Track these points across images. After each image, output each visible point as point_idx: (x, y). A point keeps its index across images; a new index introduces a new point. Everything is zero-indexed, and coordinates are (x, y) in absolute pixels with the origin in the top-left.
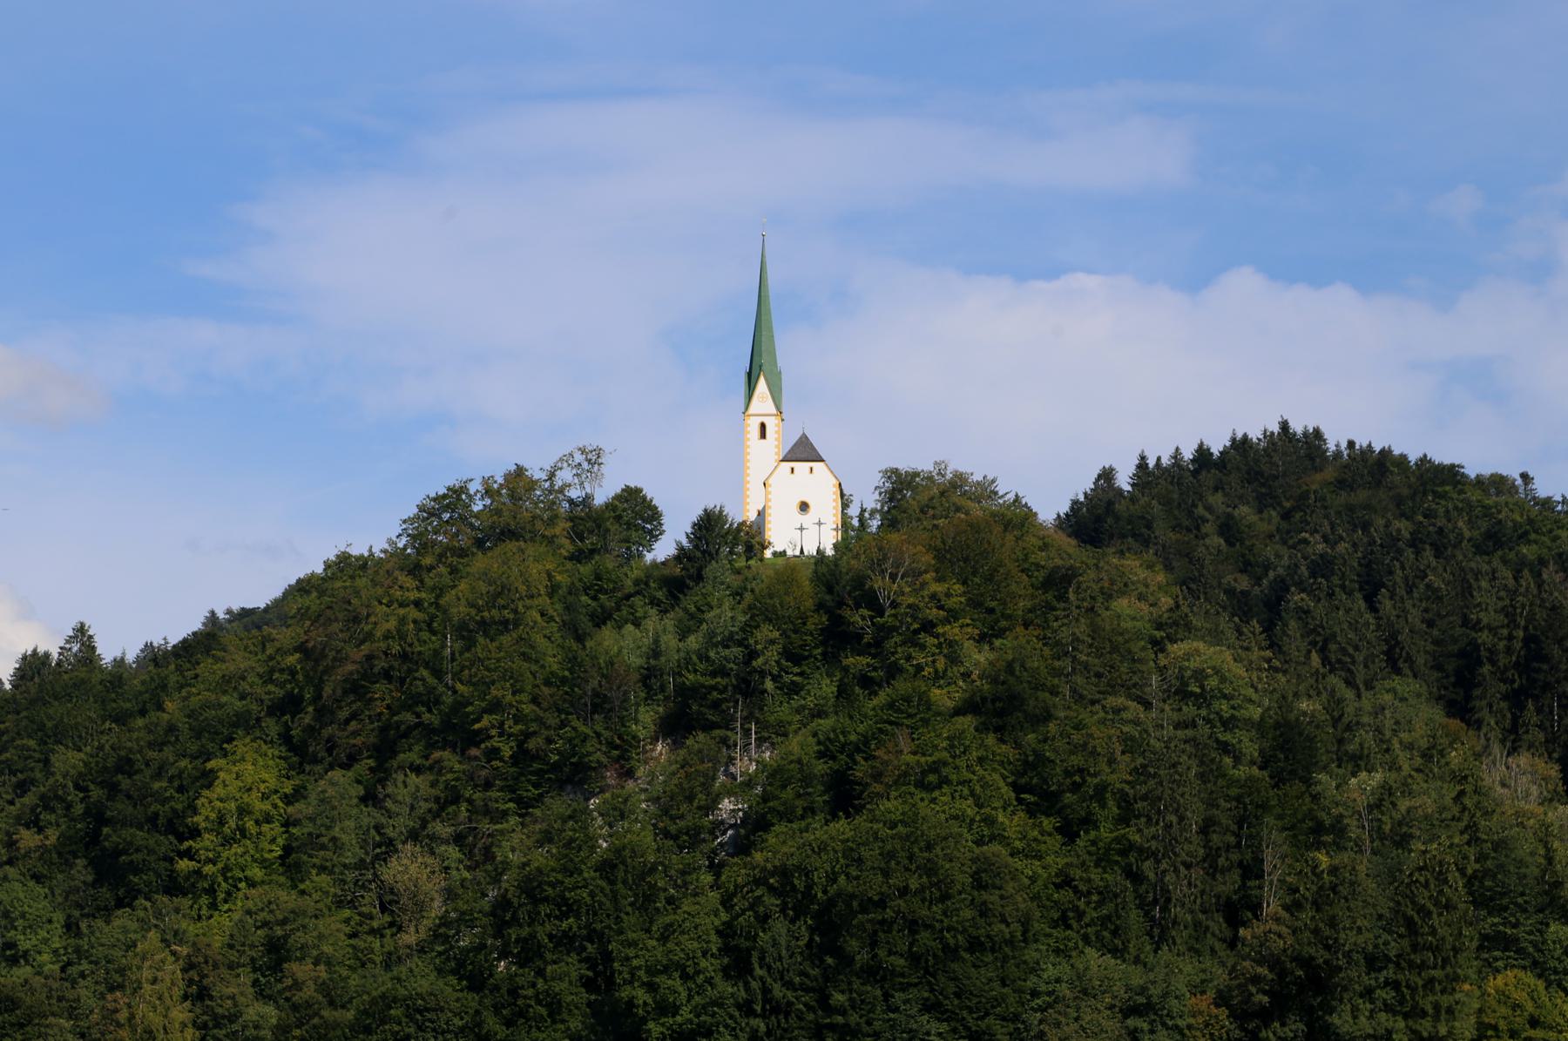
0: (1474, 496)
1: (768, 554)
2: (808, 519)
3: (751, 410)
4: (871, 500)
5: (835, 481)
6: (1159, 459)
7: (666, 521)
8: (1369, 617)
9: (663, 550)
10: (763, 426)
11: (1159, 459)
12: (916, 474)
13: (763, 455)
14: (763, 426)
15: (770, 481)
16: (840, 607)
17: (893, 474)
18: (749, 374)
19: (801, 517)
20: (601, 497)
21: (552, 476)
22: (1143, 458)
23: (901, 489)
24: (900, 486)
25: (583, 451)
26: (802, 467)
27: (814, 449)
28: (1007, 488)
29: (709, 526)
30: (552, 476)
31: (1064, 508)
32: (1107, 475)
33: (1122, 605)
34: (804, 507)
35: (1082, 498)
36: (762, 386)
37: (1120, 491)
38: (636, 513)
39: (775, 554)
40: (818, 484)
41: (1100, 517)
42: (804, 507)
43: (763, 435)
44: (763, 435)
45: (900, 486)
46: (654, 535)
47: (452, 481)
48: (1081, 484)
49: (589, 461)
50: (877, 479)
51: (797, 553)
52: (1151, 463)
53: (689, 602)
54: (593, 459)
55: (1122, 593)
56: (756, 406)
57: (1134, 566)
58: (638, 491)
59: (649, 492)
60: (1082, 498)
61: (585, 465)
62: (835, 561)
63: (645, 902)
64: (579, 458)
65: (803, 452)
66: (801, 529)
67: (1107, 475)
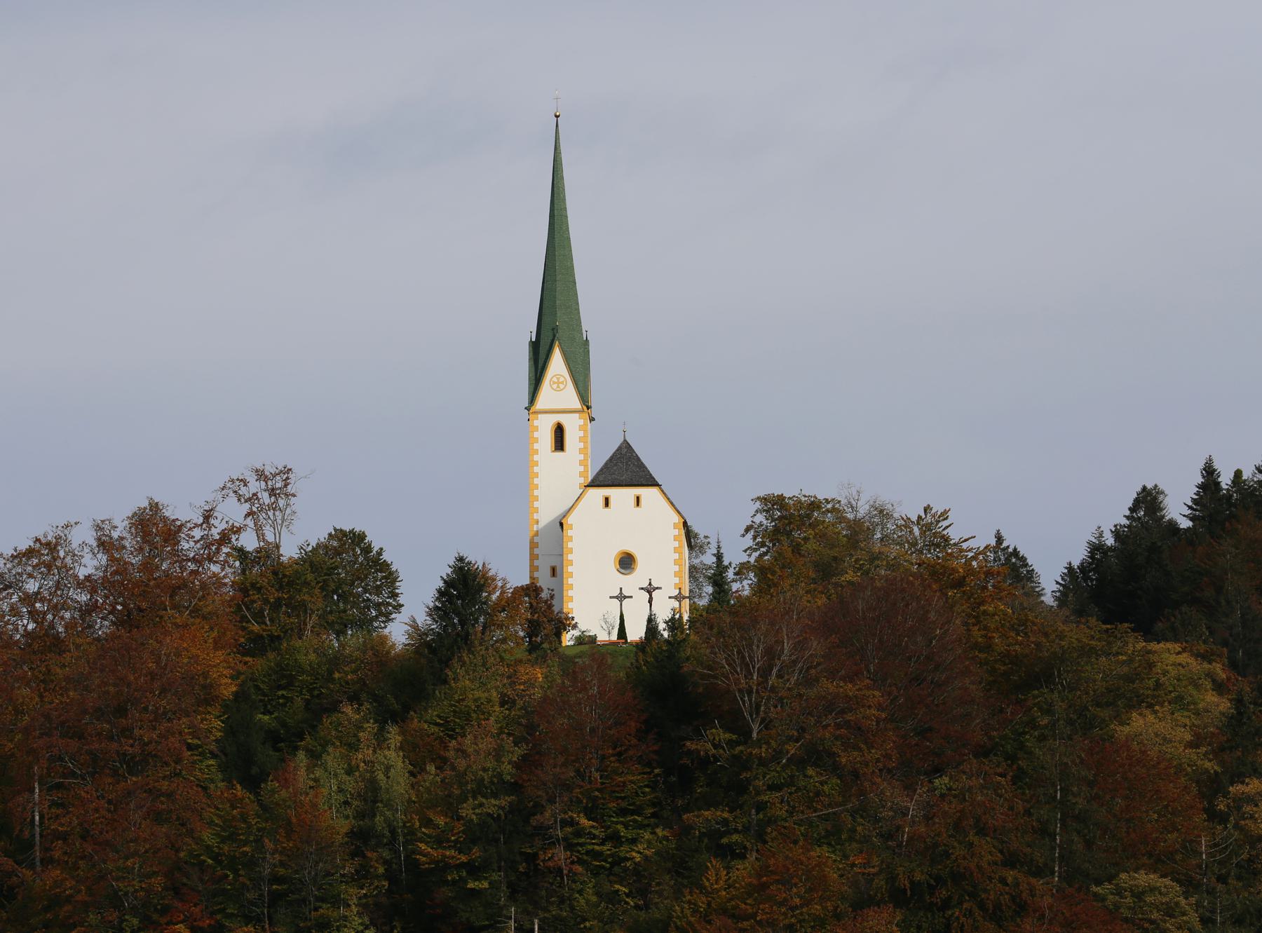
1: (568, 639)
2: (632, 583)
3: (541, 403)
4: (737, 551)
5: (676, 519)
6: (1238, 474)
7: (403, 588)
10: (559, 431)
11: (1238, 474)
12: (815, 505)
13: (558, 478)
14: (559, 431)
15: (571, 520)
17: (772, 503)
19: (623, 576)
20: (290, 551)
21: (207, 516)
22: (1209, 472)
23: (791, 526)
25: (261, 475)
26: (622, 496)
27: (641, 466)
28: (971, 530)
30: (207, 516)
31: (1078, 555)
32: (1148, 500)
33: (1141, 724)
34: (627, 562)
35: (1110, 541)
36: (557, 364)
37: (1172, 526)
39: (580, 641)
41: (1141, 571)
42: (627, 562)
43: (559, 444)
44: (559, 444)
45: (791, 526)
46: (388, 610)
47: (44, 528)
48: (1110, 514)
50: (749, 512)
52: (1225, 480)
53: (424, 722)
54: (276, 488)
55: (1138, 702)
56: (546, 397)
57: (1171, 657)
58: (357, 539)
59: (376, 540)
60: (1110, 541)
61: (265, 498)
62: (674, 644)
63: (1043, 767)
64: (255, 486)
65: (623, 470)
66: (621, 597)
67: (1148, 500)
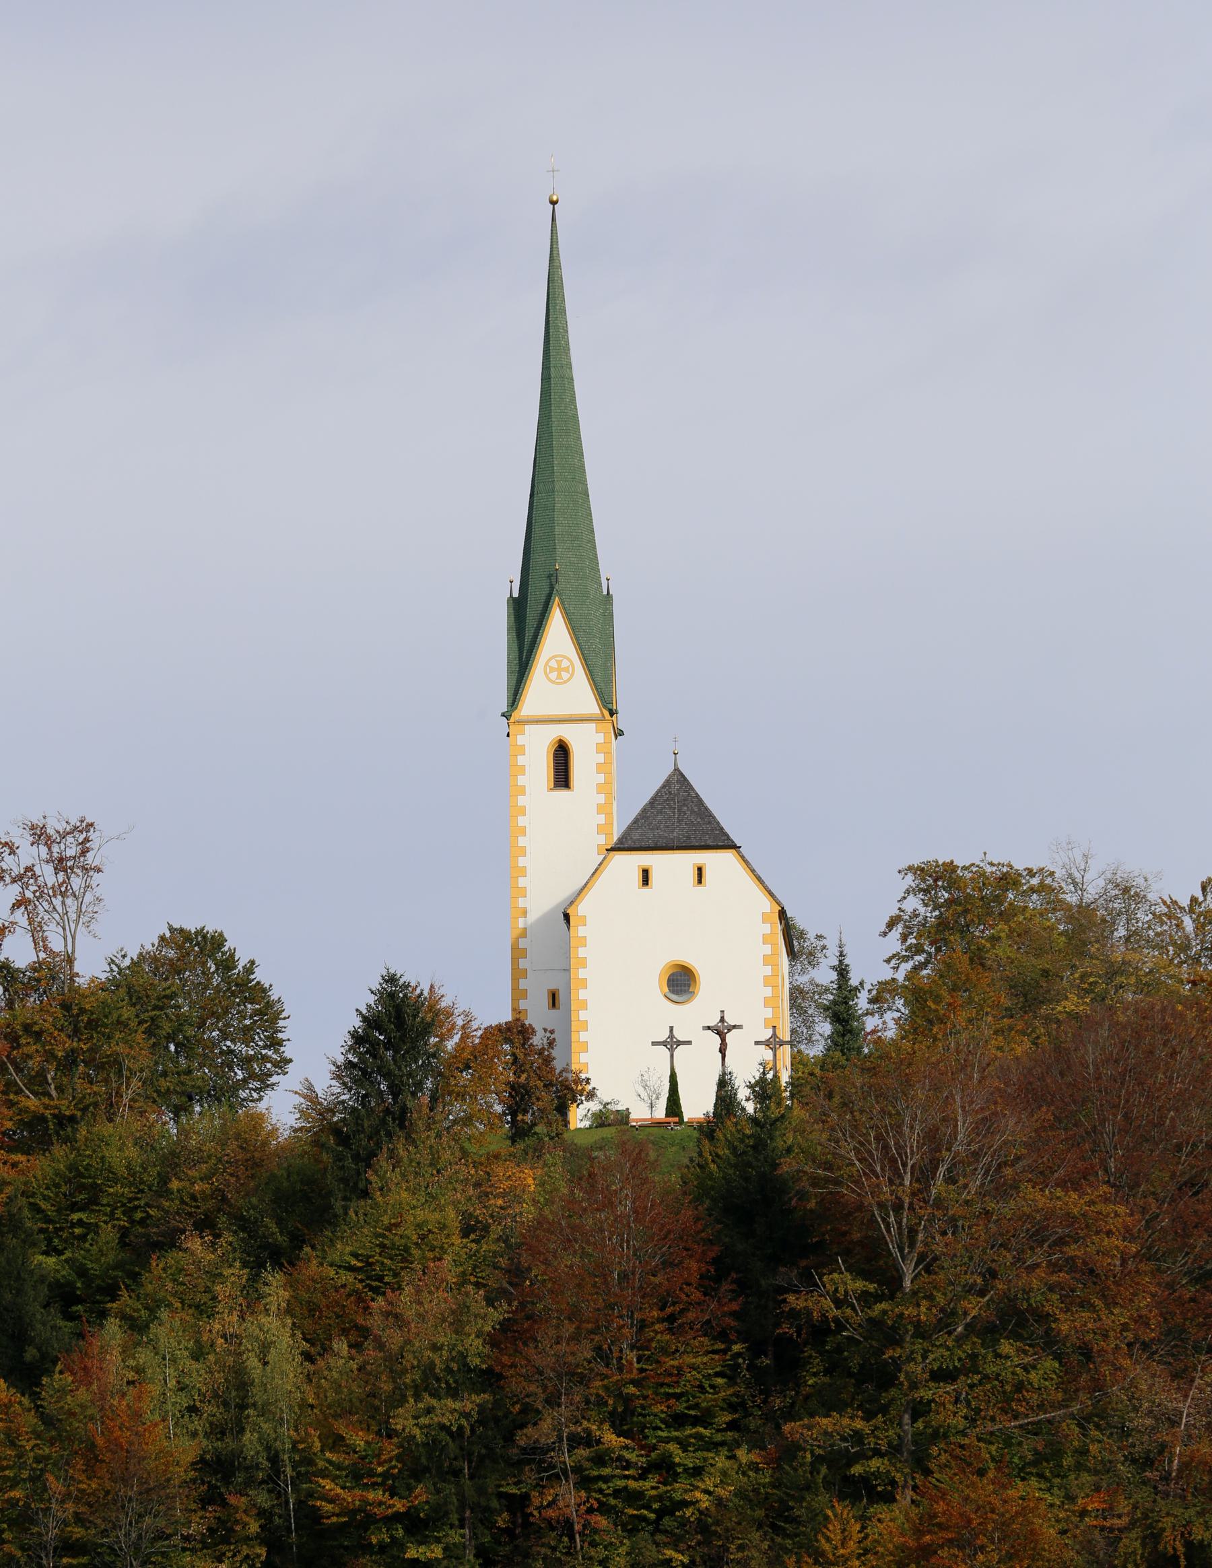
0: (642, 1136)
1: (579, 1116)
2: (691, 1018)
3: (530, 705)
4: (874, 961)
7: (292, 1030)
8: (426, 1110)
9: (281, 1109)
10: (562, 753)
14: (562, 753)
15: (582, 909)
16: (755, 1206)
17: (935, 877)
18: (518, 606)
24: (963, 911)
25: (40, 835)
26: (672, 866)
27: (705, 814)
29: (397, 1026)
34: (681, 982)
36: (557, 638)
38: (196, 1000)
40: (714, 915)
42: (681, 982)
43: (562, 776)
44: (562, 776)
45: (963, 911)
46: (265, 1068)
49: (60, 864)
50: (892, 894)
51: (660, 1113)
56: (540, 693)
61: (48, 875)
62: (764, 1125)
64: (29, 854)
65: (675, 821)
